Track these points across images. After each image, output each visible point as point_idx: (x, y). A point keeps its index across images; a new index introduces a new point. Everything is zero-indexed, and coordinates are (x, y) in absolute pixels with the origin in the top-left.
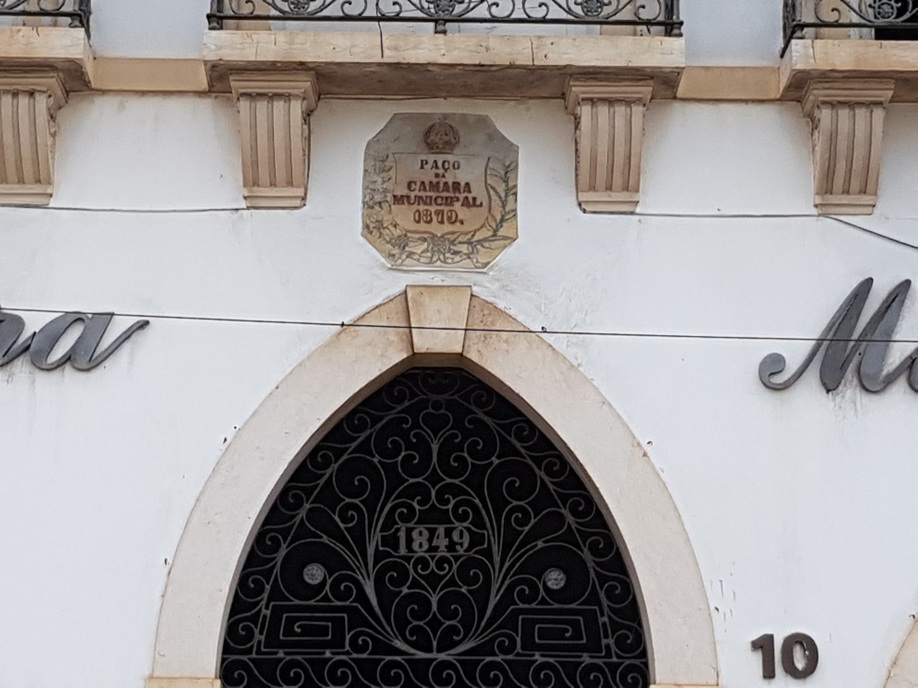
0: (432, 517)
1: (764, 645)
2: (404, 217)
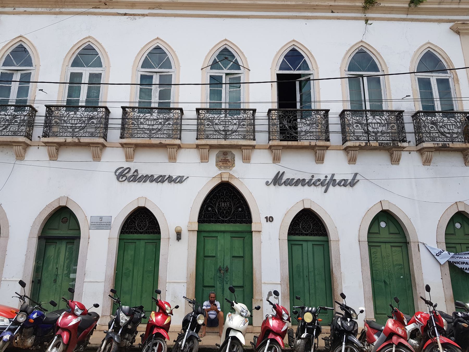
0: (225, 202)
1: (266, 218)
2: (221, 164)
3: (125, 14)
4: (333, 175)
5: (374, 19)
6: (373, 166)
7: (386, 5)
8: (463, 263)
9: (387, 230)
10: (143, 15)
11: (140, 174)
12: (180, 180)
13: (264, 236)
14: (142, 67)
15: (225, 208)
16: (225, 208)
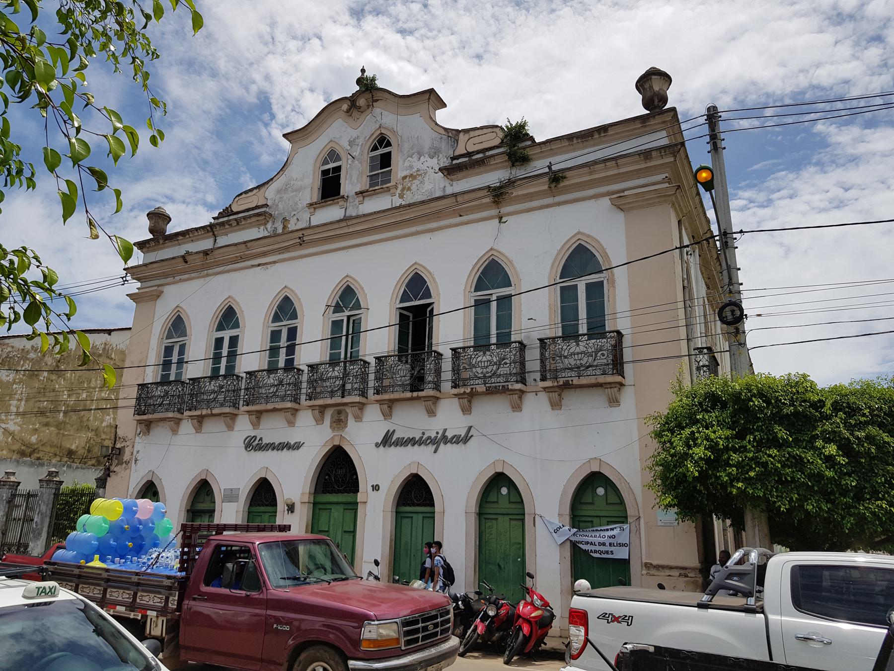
0: (341, 468)
3: (259, 265)
4: (445, 430)
5: (509, 214)
6: (491, 414)
7: (520, 193)
8: (587, 543)
9: (500, 496)
10: (275, 262)
11: (265, 441)
12: (297, 446)
13: (369, 506)
14: (273, 322)
15: (337, 474)
16: (337, 474)
